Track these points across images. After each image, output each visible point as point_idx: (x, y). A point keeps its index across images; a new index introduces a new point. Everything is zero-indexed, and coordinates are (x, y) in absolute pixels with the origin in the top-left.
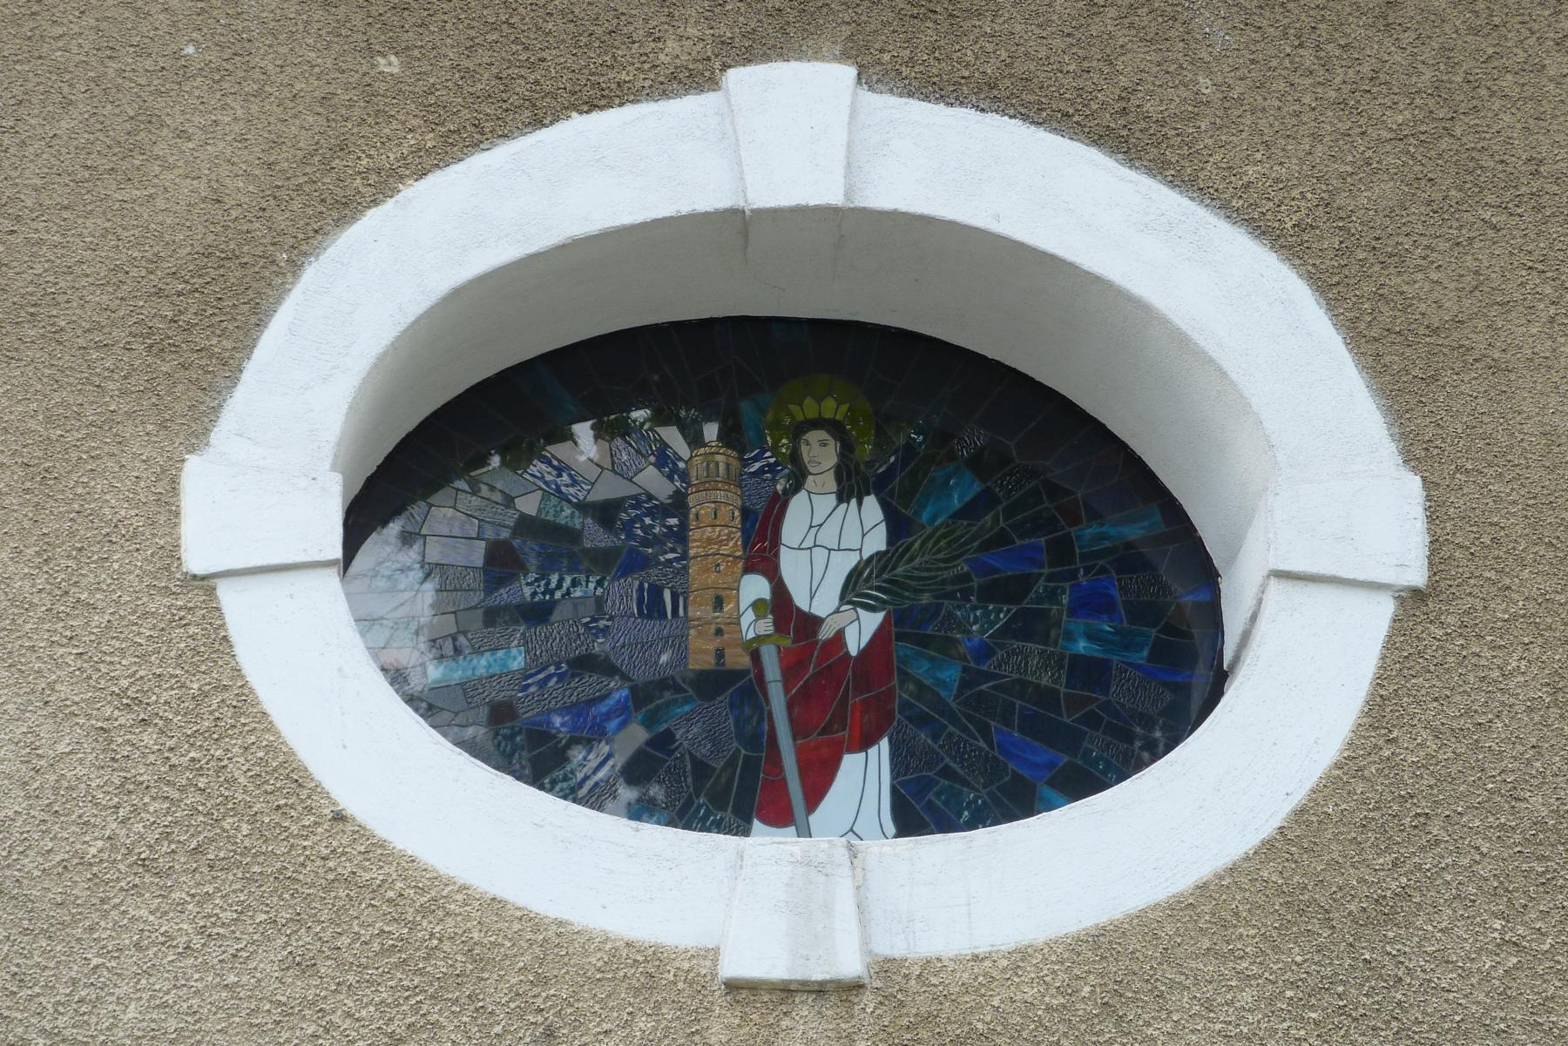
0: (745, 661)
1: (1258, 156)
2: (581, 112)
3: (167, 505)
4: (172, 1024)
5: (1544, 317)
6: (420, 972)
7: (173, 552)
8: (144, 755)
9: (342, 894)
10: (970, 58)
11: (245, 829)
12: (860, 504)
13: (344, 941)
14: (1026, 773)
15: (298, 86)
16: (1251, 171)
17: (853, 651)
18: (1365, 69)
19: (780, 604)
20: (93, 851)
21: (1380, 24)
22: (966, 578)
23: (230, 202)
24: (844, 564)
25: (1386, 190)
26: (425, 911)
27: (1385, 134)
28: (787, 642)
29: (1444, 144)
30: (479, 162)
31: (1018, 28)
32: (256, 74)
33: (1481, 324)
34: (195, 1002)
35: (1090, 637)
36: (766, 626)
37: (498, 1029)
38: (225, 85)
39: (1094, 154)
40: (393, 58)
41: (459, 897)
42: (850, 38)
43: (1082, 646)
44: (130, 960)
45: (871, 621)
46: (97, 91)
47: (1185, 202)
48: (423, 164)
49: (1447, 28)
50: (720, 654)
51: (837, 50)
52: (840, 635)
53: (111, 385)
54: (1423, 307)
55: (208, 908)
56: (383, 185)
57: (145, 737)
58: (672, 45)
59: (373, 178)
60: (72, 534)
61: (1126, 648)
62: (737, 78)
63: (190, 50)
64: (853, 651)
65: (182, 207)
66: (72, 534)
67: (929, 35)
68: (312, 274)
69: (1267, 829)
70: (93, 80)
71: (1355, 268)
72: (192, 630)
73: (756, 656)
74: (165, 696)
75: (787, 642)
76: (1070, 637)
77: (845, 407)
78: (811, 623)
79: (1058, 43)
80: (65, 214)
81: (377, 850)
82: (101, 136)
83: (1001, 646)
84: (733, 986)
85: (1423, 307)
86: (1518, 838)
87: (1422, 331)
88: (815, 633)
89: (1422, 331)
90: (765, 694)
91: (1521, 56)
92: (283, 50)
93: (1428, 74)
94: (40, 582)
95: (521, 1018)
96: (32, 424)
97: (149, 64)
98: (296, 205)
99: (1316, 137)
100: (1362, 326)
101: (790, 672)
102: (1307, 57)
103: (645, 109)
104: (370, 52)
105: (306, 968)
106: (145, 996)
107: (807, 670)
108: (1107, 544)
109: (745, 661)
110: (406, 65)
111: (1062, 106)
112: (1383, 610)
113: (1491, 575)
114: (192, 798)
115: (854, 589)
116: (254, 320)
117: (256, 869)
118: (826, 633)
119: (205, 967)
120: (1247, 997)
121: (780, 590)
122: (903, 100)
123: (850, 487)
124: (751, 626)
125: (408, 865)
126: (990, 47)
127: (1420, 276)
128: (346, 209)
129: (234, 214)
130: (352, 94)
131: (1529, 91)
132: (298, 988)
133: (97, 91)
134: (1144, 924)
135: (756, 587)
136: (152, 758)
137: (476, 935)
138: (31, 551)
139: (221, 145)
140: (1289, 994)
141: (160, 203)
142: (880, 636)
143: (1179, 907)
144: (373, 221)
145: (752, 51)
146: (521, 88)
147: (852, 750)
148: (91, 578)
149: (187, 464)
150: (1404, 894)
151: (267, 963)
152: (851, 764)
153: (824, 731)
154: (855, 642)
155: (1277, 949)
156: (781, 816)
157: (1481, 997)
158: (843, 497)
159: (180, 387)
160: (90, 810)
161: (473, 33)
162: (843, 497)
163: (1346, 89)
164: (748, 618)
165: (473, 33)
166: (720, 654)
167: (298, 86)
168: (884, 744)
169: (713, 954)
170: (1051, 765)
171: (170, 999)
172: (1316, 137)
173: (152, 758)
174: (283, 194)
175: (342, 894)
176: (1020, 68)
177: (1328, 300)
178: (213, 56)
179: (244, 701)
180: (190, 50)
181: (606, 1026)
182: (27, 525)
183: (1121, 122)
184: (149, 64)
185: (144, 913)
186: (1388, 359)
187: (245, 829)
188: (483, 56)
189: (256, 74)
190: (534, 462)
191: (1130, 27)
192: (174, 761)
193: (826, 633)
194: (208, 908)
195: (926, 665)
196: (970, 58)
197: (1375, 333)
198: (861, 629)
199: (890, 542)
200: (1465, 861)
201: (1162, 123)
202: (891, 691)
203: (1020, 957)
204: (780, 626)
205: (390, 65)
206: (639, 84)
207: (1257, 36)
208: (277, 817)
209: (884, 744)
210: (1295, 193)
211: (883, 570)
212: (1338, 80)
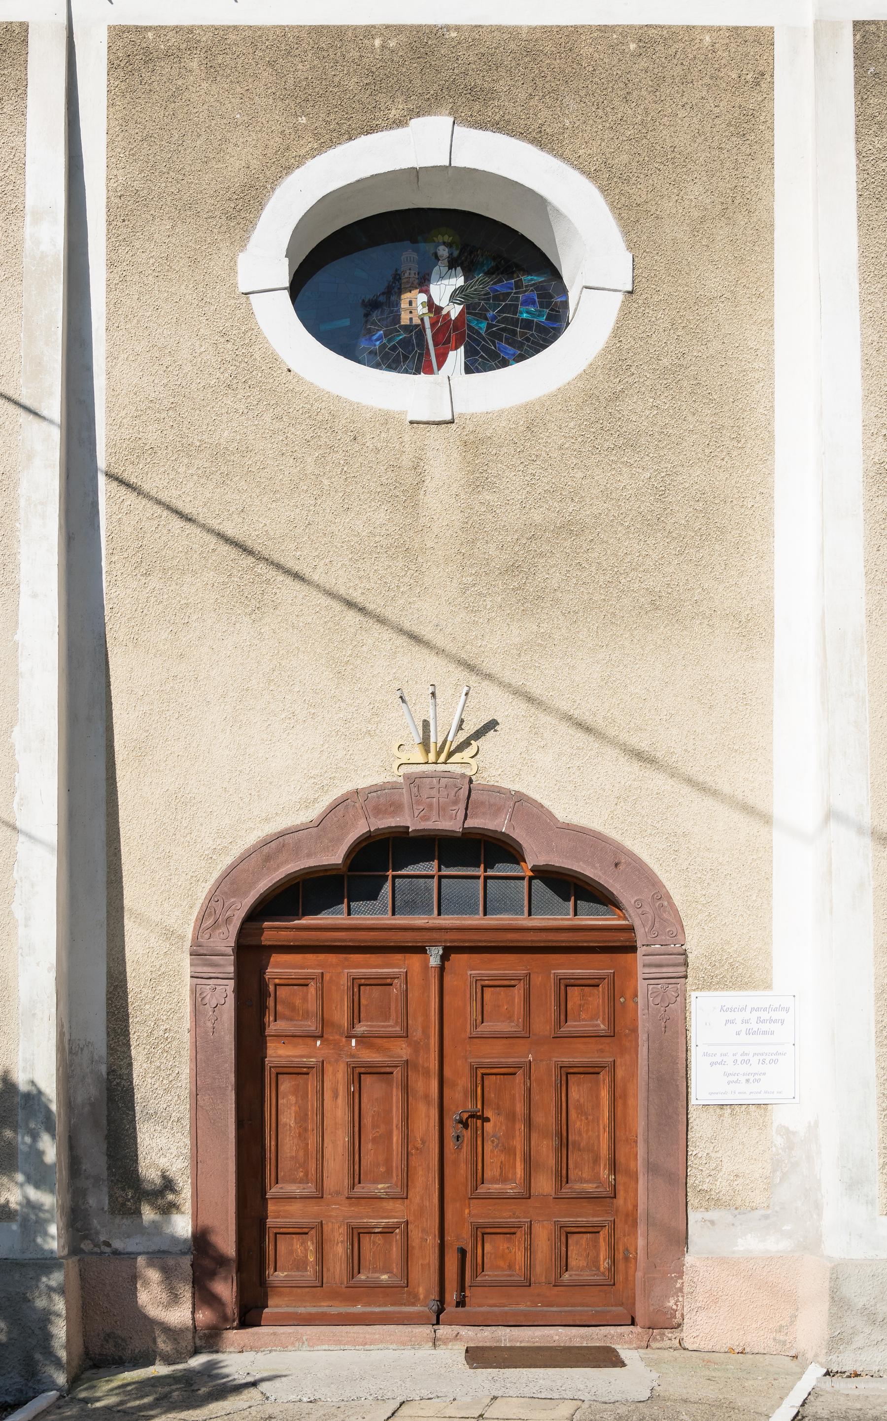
0: (419, 322)
1: (583, 146)
3: (233, 270)
4: (238, 437)
5: (674, 200)
6: (315, 420)
7: (235, 286)
8: (228, 352)
9: (290, 395)
10: (490, 114)
11: (260, 375)
12: (455, 270)
13: (291, 410)
14: (507, 357)
15: (273, 128)
16: (581, 152)
17: (453, 318)
18: (619, 116)
19: (430, 304)
20: (213, 383)
21: (625, 100)
22: (488, 294)
23: (252, 168)
25: (625, 158)
26: (316, 400)
27: (625, 139)
28: (432, 315)
29: (644, 141)
30: (331, 152)
31: (506, 103)
32: (260, 124)
33: (654, 203)
34: (245, 430)
35: (527, 312)
36: (426, 310)
37: (339, 437)
38: (249, 128)
39: (530, 146)
40: (303, 118)
41: (326, 395)
42: (452, 108)
43: (525, 316)
44: (225, 418)
45: (459, 308)
46: (208, 131)
47: (559, 162)
48: (314, 153)
49: (646, 101)
50: (411, 319)
51: (447, 112)
52: (448, 313)
53: (215, 230)
54: (635, 197)
55: (249, 401)
56: (301, 161)
57: (228, 346)
58: (393, 112)
59: (297, 159)
60: (204, 280)
61: (539, 316)
62: (415, 122)
63: (238, 116)
64: (453, 318)
65: (237, 170)
66: (204, 280)
67: (477, 107)
68: (278, 191)
69: (580, 371)
70: (207, 127)
71: (613, 184)
72: (242, 311)
73: (422, 320)
74: (234, 332)
75: (432, 315)
76: (521, 313)
77: (451, 238)
78: (439, 309)
79: (519, 109)
80: (199, 173)
82: (210, 146)
83: (499, 316)
84: (411, 422)
85: (635, 197)
86: (658, 372)
87: (634, 205)
88: (470, 354)
89: (634, 205)
90: (425, 332)
91: (670, 111)
92: (268, 116)
93: (640, 117)
94: (194, 296)
95: (346, 434)
96: (190, 244)
97: (225, 121)
98: (273, 168)
99: (602, 140)
100: (615, 204)
101: (433, 325)
102: (600, 112)
103: (385, 133)
104: (296, 115)
106: (230, 429)
108: (533, 282)
109: (419, 322)
110: (308, 120)
111: (520, 130)
112: (620, 297)
113: (654, 286)
114: (243, 365)
115: (453, 298)
116: (260, 207)
117: (263, 387)
118: (444, 312)
119: (248, 419)
120: (572, 425)
121: (430, 298)
122: (469, 129)
123: (452, 264)
124: (422, 310)
126: (497, 110)
127: (634, 186)
128: (289, 169)
129: (253, 172)
130: (290, 130)
131: (672, 123)
132: (278, 425)
133: (208, 131)
134: (541, 402)
135: (423, 297)
136: (230, 352)
137: (332, 408)
138: (191, 286)
139: (249, 149)
140: (585, 423)
141: (230, 169)
142: (461, 313)
143: (552, 396)
144: (297, 174)
145: (419, 113)
146: (345, 127)
147: (451, 350)
148: (210, 294)
149: (240, 257)
150: (622, 391)
151: (268, 417)
152: (452, 354)
153: (443, 344)
154: (454, 316)
155: (582, 409)
156: (429, 371)
157: (645, 424)
158: (450, 268)
159: (238, 231)
160: (211, 370)
161: (329, 108)
162: (450, 268)
163: (612, 123)
164: (420, 307)
165: (329, 108)
166: (411, 319)
167: (273, 128)
168: (462, 347)
169: (405, 413)
170: (514, 355)
171: (238, 429)
172: (602, 140)
173: (230, 352)
174: (268, 165)
175: (290, 395)
176: (506, 117)
177: (604, 195)
178: (245, 118)
180: (238, 116)
181: (372, 436)
182: (190, 277)
183: (539, 135)
184: (225, 121)
185: (229, 402)
186: (623, 215)
187: (260, 375)
188: (332, 116)
189: (260, 124)
190: (408, 322)
191: (543, 102)
192: (237, 353)
193: (444, 312)
194: (249, 401)
195: (476, 322)
196: (490, 114)
197: (619, 206)
198: (455, 311)
199: (465, 282)
200: (642, 380)
201: (552, 136)
202: (465, 330)
204: (430, 311)
205: (303, 120)
206: (383, 125)
207: (584, 105)
208: (269, 371)
209: (462, 347)
210: (595, 159)
211: (462, 291)
212: (610, 120)
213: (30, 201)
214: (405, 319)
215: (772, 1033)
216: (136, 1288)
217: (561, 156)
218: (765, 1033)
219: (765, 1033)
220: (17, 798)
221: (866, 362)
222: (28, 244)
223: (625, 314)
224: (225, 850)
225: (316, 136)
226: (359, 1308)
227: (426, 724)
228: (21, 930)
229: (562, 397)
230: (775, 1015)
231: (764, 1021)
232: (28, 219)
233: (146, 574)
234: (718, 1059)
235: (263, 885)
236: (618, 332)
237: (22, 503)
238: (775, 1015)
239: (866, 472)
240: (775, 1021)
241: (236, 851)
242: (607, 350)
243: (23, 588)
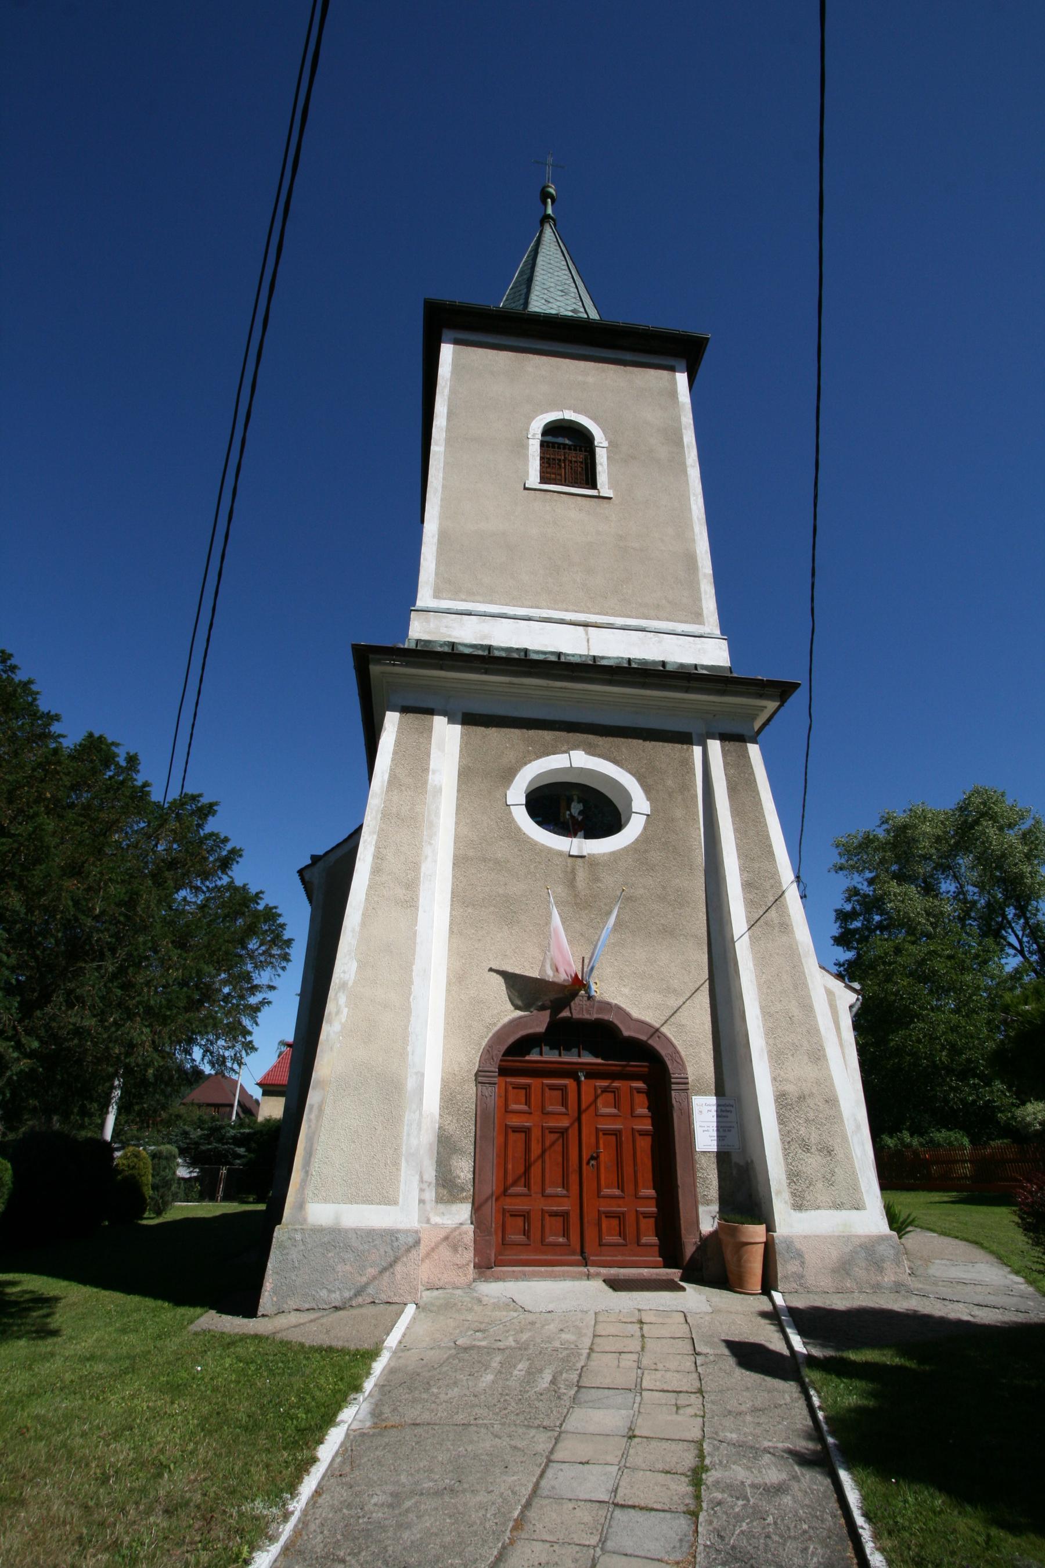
2: (416, 925)
19: (571, 815)
24: (578, 811)
56: (530, 761)
81: (529, 838)
105: (520, 851)
107: (216, 1148)
115: (580, 813)
123: (579, 802)
124: (567, 817)
125: (532, 839)
128: (526, 764)
132: (519, 853)
134: (618, 851)
135: (568, 812)
143: (622, 849)
144: (529, 766)
151: (516, 850)
179: (513, 820)
198: (580, 818)
203: (604, 854)
213: (431, 767)
214: (562, 820)
215: (727, 1117)
216: (1017, 1273)
217: (622, 767)
218: (724, 1117)
219: (724, 1117)
220: (412, 997)
221: (737, 844)
222: (430, 781)
223: (647, 822)
224: (495, 1024)
225: (535, 753)
226: (619, 1258)
227: (491, 970)
228: (410, 1056)
229: (626, 850)
230: (728, 1108)
231: (723, 1111)
232: (430, 773)
233: (467, 907)
234: (706, 1129)
235: (511, 1040)
236: (645, 828)
237: (422, 875)
238: (728, 1108)
239: (742, 885)
240: (728, 1111)
241: (499, 1025)
242: (642, 834)
243: (420, 908)
